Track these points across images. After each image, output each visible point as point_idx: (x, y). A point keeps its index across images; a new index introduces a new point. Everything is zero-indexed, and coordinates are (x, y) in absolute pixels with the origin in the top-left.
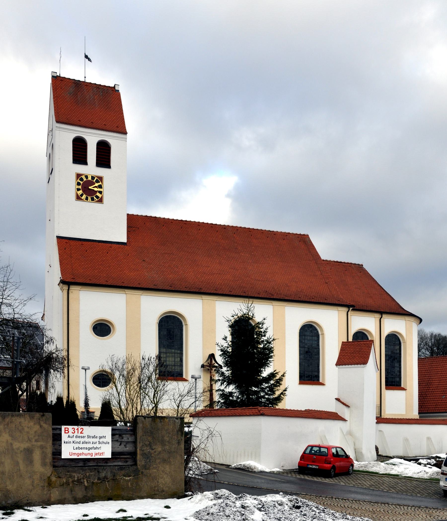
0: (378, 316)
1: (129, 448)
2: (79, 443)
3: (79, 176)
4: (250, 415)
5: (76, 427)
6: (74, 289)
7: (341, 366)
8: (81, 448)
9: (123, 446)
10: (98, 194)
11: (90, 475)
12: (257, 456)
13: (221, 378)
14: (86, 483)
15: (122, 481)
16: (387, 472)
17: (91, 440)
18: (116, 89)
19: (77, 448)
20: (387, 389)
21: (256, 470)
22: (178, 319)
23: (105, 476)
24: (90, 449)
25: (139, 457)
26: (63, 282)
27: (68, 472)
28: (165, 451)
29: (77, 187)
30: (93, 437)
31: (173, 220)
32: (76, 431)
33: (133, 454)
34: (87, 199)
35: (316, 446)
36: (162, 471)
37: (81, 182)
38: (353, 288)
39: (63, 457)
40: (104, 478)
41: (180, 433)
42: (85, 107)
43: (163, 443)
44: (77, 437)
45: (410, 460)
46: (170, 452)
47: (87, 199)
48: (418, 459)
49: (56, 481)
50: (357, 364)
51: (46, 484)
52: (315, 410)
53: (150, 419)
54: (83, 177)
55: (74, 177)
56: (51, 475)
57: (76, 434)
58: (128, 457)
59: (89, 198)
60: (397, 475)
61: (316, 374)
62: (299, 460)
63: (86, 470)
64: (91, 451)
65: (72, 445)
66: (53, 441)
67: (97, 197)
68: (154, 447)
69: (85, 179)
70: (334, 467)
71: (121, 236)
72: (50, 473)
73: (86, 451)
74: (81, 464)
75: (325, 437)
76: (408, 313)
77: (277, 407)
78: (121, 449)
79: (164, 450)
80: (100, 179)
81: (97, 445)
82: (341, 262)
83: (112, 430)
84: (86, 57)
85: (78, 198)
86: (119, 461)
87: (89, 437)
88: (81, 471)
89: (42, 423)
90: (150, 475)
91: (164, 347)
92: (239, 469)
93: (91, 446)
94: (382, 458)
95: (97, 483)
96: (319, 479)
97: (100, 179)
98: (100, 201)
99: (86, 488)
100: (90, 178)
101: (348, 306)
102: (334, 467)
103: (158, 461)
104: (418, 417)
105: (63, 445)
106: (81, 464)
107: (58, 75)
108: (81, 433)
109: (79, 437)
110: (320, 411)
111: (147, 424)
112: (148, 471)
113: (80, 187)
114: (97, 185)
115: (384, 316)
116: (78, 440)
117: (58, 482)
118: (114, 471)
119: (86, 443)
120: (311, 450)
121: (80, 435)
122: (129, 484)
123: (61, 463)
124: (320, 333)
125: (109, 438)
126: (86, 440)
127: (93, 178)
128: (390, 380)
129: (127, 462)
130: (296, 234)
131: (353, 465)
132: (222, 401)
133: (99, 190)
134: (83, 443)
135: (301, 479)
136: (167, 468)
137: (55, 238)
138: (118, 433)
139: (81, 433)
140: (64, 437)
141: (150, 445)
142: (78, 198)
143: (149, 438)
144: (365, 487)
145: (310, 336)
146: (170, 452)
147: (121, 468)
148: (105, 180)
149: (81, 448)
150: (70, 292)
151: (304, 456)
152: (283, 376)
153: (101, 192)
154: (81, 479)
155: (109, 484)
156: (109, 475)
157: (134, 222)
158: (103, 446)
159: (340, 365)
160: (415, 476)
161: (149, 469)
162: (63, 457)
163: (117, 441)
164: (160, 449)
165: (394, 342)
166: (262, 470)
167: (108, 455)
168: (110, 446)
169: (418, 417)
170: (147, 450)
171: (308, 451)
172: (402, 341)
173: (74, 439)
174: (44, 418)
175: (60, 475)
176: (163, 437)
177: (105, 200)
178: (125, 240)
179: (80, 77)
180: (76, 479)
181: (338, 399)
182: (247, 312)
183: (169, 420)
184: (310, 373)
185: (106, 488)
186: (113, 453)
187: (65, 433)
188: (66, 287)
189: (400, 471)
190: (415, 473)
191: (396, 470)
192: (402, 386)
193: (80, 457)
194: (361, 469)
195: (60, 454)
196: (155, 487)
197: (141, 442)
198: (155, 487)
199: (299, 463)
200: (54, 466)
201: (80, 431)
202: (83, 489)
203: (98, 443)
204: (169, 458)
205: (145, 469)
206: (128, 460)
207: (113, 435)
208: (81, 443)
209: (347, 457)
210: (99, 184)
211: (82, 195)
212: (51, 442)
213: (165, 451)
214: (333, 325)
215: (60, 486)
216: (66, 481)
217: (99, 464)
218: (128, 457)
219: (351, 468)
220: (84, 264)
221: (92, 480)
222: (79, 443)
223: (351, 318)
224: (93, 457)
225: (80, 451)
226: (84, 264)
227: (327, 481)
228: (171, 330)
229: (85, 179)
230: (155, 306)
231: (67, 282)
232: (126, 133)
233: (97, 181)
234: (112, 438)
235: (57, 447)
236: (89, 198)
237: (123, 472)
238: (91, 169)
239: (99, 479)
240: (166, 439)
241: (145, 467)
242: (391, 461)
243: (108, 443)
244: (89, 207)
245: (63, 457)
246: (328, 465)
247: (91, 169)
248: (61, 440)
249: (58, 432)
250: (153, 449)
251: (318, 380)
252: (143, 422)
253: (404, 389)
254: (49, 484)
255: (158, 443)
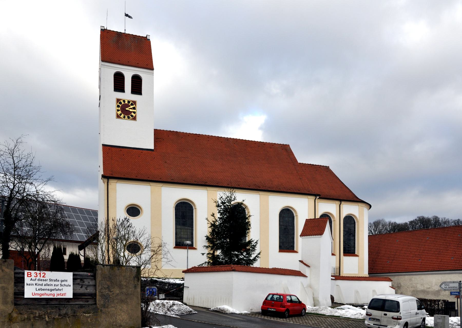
0: (338, 203)
1: (90, 290)
2: (42, 285)
3: (118, 100)
4: (225, 271)
5: (38, 272)
6: (112, 182)
7: (304, 237)
8: (44, 290)
9: (84, 288)
10: (133, 114)
11: (51, 311)
12: (230, 302)
13: (211, 245)
14: (47, 319)
15: (82, 317)
16: (332, 314)
17: (53, 283)
18: (148, 38)
19: (39, 290)
20: (344, 255)
21: (228, 312)
22: (190, 204)
23: (66, 313)
24: (51, 290)
25: (98, 297)
26: (103, 176)
27: (30, 309)
28: (123, 293)
29: (117, 108)
30: (55, 281)
31: (190, 133)
32: (39, 275)
33: (93, 296)
34: (124, 117)
35: (277, 294)
36: (120, 310)
37: (120, 105)
38: (323, 183)
39: (25, 297)
40: (65, 315)
41: (136, 279)
42: (125, 52)
43: (120, 287)
44: (39, 280)
45: (357, 306)
46: (127, 294)
47: (124, 117)
48: (364, 306)
49: (17, 317)
50: (316, 235)
51: (7, 320)
52: (280, 269)
53: (109, 267)
54: (122, 101)
55: (115, 101)
56: (12, 312)
57: (38, 277)
58: (89, 297)
59: (126, 117)
60: (339, 317)
61: (292, 244)
62: (262, 305)
63: (47, 307)
64: (53, 292)
65: (35, 287)
66: (15, 283)
67: (132, 116)
68: (112, 290)
69: (123, 103)
70: (288, 310)
71: (150, 144)
72: (12, 310)
73: (49, 292)
74: (44, 303)
75: (288, 288)
76: (358, 200)
77: (252, 266)
78: (82, 290)
79: (122, 293)
80: (134, 103)
81: (59, 287)
82: (313, 165)
83: (74, 275)
84: (127, 15)
85: (118, 116)
86: (81, 301)
87: (51, 280)
88: (43, 308)
89: (4, 268)
90: (109, 312)
91: (180, 225)
92: (216, 311)
93: (53, 287)
94: (335, 304)
95: (58, 319)
96: (275, 319)
97: (134, 103)
98: (134, 119)
99: (47, 323)
100: (126, 102)
101: (315, 195)
102: (288, 310)
103: (116, 301)
104: (367, 276)
105: (26, 287)
106: (44, 303)
107: (105, 28)
108: (43, 277)
109: (41, 280)
110: (285, 269)
111: (106, 271)
112: (106, 309)
113: (119, 109)
114: (131, 107)
115: (342, 203)
116: (40, 282)
117: (19, 318)
118: (75, 309)
119: (49, 285)
120: (272, 297)
121: (42, 278)
122: (89, 320)
123: (24, 302)
124: (295, 215)
125: (70, 282)
126: (48, 282)
127: (129, 102)
128: (347, 249)
129: (88, 301)
130: (281, 144)
131: (305, 309)
132: (211, 262)
133: (133, 110)
134: (45, 285)
135: (263, 320)
136: (125, 307)
137: (101, 146)
138: (79, 277)
139: (43, 277)
140: (27, 280)
141: (108, 288)
142: (118, 116)
143: (107, 283)
144: (308, 325)
145: (287, 216)
146: (127, 294)
147: (81, 306)
148: (138, 104)
149: (44, 290)
150: (109, 184)
151: (266, 302)
152: (256, 243)
153: (134, 113)
154: (42, 315)
155: (69, 320)
156: (70, 312)
157: (159, 135)
158: (64, 288)
159: (303, 236)
160: (353, 317)
161: (107, 307)
162: (26, 296)
163: (79, 284)
164: (118, 292)
165: (350, 223)
166: (233, 312)
167: (70, 295)
168: (72, 287)
169: (367, 276)
170: (106, 292)
171: (269, 298)
172: (356, 221)
173: (37, 282)
174: (6, 264)
175: (22, 312)
176: (120, 282)
177: (138, 118)
178: (152, 148)
179: (121, 30)
180: (37, 315)
181: (301, 261)
182: (230, 195)
183: (126, 269)
184: (287, 245)
185: (67, 322)
186: (74, 294)
187: (28, 276)
188: (106, 180)
189: (342, 313)
190: (352, 315)
191: (339, 313)
192: (356, 253)
193: (42, 297)
194: (313, 312)
195: (23, 294)
196: (113, 322)
197: (100, 285)
198: (113, 322)
199: (262, 307)
200: (16, 304)
201: (42, 275)
202: (45, 323)
203: (59, 285)
204: (127, 299)
205: (104, 308)
206: (89, 300)
207: (74, 279)
208: (43, 285)
209: (300, 302)
210: (133, 106)
211: (121, 115)
212: (13, 284)
213: (123, 293)
214: (304, 208)
215: (21, 321)
216: (28, 317)
217: (62, 303)
218: (89, 297)
219: (303, 311)
220: (121, 164)
221: (53, 316)
222: (42, 285)
223: (318, 204)
224: (55, 297)
225: (43, 292)
226: (121, 164)
227: (281, 320)
228: (184, 212)
229: (123, 103)
230: (173, 194)
231: (107, 177)
232: (153, 69)
233: (132, 104)
234: (73, 282)
235: (19, 288)
236: (126, 117)
237: (83, 310)
238: (127, 95)
239: (60, 315)
240: (124, 283)
241: (104, 306)
242: (342, 307)
243: (70, 286)
244: (126, 123)
245: (25, 297)
246: (283, 309)
247: (127, 95)
248: (24, 283)
249: (21, 275)
250: (111, 292)
251: (294, 249)
252: (101, 269)
253: (357, 256)
254: (10, 319)
255: (116, 287)
